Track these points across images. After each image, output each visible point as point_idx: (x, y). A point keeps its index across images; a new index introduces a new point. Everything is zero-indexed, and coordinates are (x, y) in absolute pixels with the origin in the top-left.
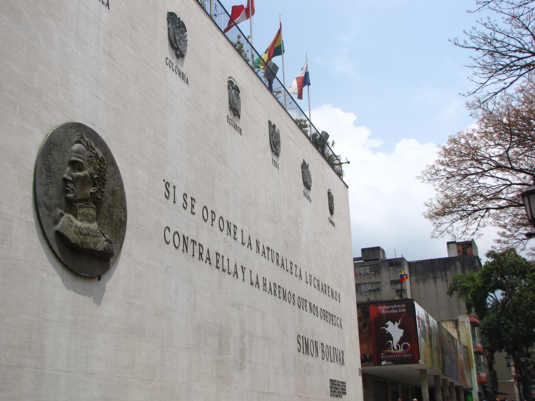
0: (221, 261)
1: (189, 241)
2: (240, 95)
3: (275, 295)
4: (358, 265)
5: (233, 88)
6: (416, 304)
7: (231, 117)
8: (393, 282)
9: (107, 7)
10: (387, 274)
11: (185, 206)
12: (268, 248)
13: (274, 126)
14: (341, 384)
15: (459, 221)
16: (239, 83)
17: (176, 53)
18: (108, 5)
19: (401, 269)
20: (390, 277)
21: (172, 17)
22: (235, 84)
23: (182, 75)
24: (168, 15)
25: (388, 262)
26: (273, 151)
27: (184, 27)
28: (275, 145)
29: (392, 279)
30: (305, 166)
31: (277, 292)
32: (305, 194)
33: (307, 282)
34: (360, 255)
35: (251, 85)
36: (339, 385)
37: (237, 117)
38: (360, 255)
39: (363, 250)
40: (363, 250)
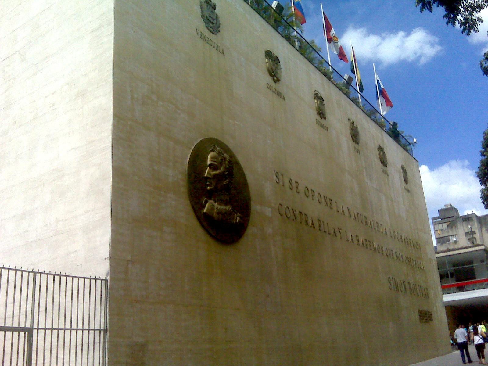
0: (322, 226)
1: (298, 212)
2: (324, 102)
3: (367, 248)
4: (437, 223)
5: (318, 97)
6: (333, 29)
7: (318, 118)
8: (467, 234)
9: (223, 54)
10: (462, 227)
11: (291, 188)
12: (358, 213)
13: (353, 123)
14: (428, 313)
15: (319, 229)
16: (322, 93)
17: (274, 79)
18: (223, 53)
19: (473, 223)
20: (464, 230)
21: (269, 54)
22: (319, 95)
23: (279, 94)
24: (265, 53)
25: (462, 218)
26: (353, 140)
27: (278, 59)
28: (355, 136)
29: (466, 231)
30: (380, 149)
31: (368, 246)
32: (383, 171)
33: (392, 237)
34: (437, 215)
35: (390, 145)
36: (426, 314)
37: (323, 119)
38: (437, 215)
39: (439, 211)
40: (439, 211)
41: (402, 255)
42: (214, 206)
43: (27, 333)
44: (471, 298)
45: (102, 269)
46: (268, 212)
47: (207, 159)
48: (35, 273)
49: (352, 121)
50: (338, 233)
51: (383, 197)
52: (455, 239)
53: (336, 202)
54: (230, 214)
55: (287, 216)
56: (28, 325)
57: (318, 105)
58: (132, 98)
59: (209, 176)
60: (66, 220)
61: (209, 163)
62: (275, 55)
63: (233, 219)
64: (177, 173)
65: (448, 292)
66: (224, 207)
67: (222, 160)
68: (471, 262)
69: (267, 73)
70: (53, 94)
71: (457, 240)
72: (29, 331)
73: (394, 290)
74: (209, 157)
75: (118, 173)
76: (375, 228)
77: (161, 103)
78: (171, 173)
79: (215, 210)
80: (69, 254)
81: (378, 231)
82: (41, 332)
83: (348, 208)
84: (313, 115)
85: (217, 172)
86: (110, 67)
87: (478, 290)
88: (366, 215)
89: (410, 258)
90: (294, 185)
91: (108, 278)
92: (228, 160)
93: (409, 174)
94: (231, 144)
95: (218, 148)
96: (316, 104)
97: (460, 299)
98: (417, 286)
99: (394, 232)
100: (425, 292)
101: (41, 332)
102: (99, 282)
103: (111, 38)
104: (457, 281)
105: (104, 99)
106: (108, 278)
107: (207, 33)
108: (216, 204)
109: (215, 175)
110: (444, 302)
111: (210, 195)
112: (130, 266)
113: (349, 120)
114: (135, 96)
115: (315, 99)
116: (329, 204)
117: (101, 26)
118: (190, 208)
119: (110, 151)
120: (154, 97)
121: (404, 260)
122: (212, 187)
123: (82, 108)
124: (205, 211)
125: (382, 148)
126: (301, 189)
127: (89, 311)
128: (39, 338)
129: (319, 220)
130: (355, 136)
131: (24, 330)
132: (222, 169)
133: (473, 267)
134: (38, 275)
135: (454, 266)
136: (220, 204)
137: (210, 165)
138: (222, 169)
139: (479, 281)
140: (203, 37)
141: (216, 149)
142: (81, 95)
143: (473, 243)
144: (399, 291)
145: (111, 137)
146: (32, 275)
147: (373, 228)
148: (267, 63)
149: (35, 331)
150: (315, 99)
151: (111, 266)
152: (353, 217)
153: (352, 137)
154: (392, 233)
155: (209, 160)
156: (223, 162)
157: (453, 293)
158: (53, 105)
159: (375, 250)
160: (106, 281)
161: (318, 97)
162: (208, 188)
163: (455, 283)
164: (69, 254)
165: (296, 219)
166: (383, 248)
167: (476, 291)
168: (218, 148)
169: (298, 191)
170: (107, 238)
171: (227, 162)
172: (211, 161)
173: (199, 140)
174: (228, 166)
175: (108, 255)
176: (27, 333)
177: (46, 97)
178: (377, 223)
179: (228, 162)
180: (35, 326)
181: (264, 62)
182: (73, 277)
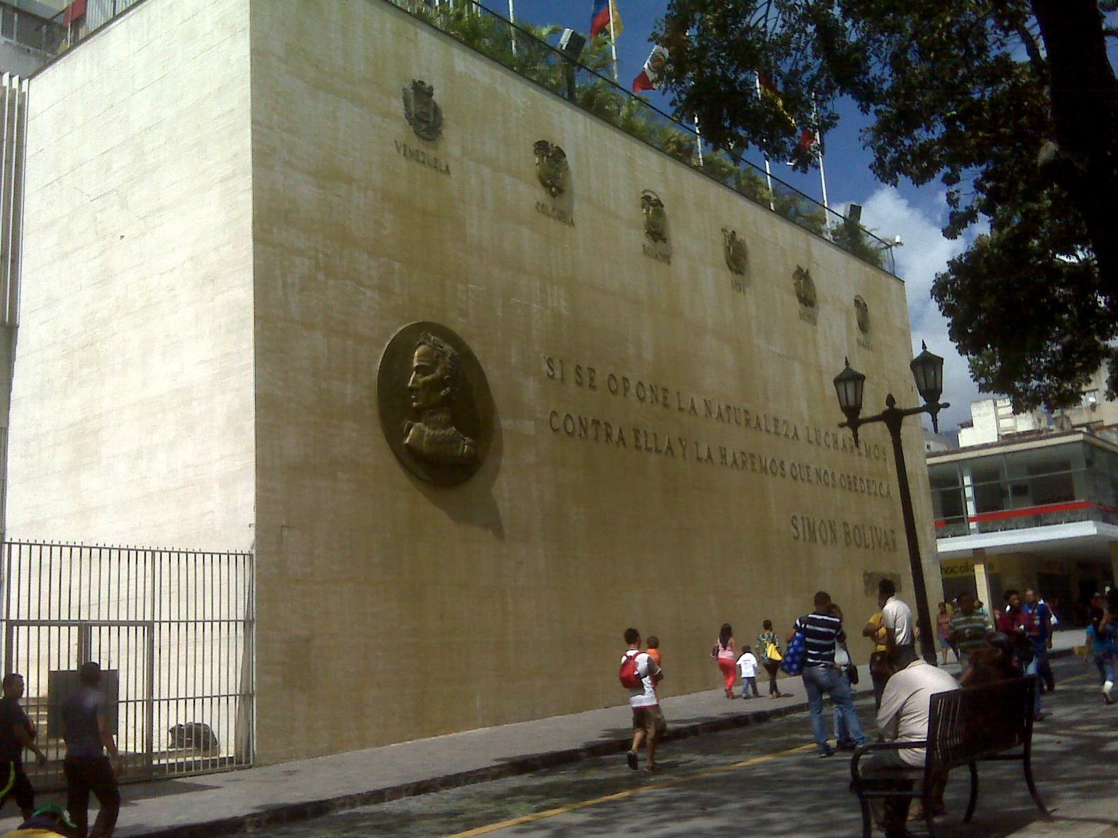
11: (579, 381)
12: (728, 408)
29: (1010, 410)
41: (833, 473)
42: (423, 432)
43: (146, 628)
44: (1082, 537)
45: (245, 540)
46: (529, 427)
47: (413, 358)
48: (153, 552)
49: (730, 231)
50: (678, 451)
51: (797, 367)
52: (1092, 400)
53: (678, 393)
54: (452, 441)
55: (566, 429)
56: (148, 618)
57: (648, 217)
58: (285, 285)
59: (415, 386)
60: (197, 466)
61: (416, 364)
62: (555, 146)
63: (458, 448)
64: (359, 390)
65: (1072, 518)
66: (442, 432)
67: (438, 357)
68: (1065, 465)
69: (538, 184)
70: (171, 271)
71: (1098, 402)
72: (149, 626)
73: (805, 539)
74: (416, 353)
75: (266, 404)
76: (768, 428)
77: (331, 282)
78: (349, 389)
79: (425, 438)
80: (204, 514)
81: (777, 434)
82: (165, 626)
83: (705, 400)
84: (637, 238)
85: (428, 378)
86: (249, 242)
87: (953, 538)
88: (747, 406)
89: (855, 478)
90: (585, 372)
91: (254, 552)
92: (449, 355)
93: (873, 311)
94: (458, 326)
95: (432, 338)
96: (645, 216)
97: (1030, 540)
98: (867, 528)
99: (817, 431)
100: (886, 538)
101: (165, 626)
102: (240, 558)
103: (249, 196)
104: (1036, 503)
105: (242, 292)
106: (254, 552)
107: (415, 144)
108: (427, 429)
109: (425, 383)
110: (938, 554)
111: (417, 415)
112: (285, 533)
113: (724, 230)
114: (289, 280)
115: (643, 207)
116: (660, 398)
117: (234, 174)
118: (382, 441)
119: (252, 371)
120: (321, 277)
121: (837, 482)
122: (420, 403)
123: (212, 300)
124: (407, 441)
125: (805, 271)
126: (600, 379)
127: (228, 594)
128: (163, 635)
129: (637, 431)
130: (736, 257)
131: (143, 623)
132: (438, 372)
133: (1070, 475)
134: (158, 554)
135: (1031, 473)
136: (434, 429)
137: (418, 369)
138: (438, 372)
139: (1004, 515)
140: (409, 154)
141: (429, 339)
142: (210, 279)
143: (1062, 427)
144: (816, 540)
145: (252, 351)
146: (149, 554)
147: (763, 428)
148: (537, 164)
149: (156, 625)
150: (643, 207)
151: (257, 536)
152: (715, 415)
153: (728, 263)
154: (812, 433)
155: (415, 359)
156: (440, 360)
157: (1017, 528)
158: (173, 290)
159: (764, 469)
160: (251, 556)
161: (652, 204)
162: (414, 404)
163: (1032, 507)
164: (204, 514)
165: (585, 432)
166: (786, 464)
167: (1063, 525)
168: (432, 338)
169: (593, 385)
170: (250, 498)
171: (447, 360)
172: (418, 361)
173: (400, 329)
174: (449, 366)
175: (253, 521)
176: (146, 628)
177: (162, 274)
178: (776, 420)
179: (450, 359)
180: (157, 618)
181: (531, 163)
182: (204, 554)
